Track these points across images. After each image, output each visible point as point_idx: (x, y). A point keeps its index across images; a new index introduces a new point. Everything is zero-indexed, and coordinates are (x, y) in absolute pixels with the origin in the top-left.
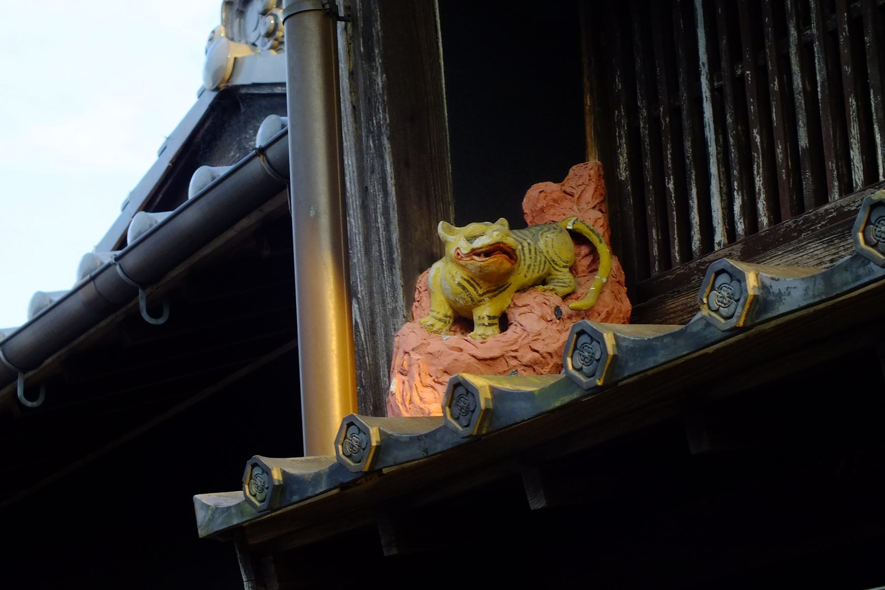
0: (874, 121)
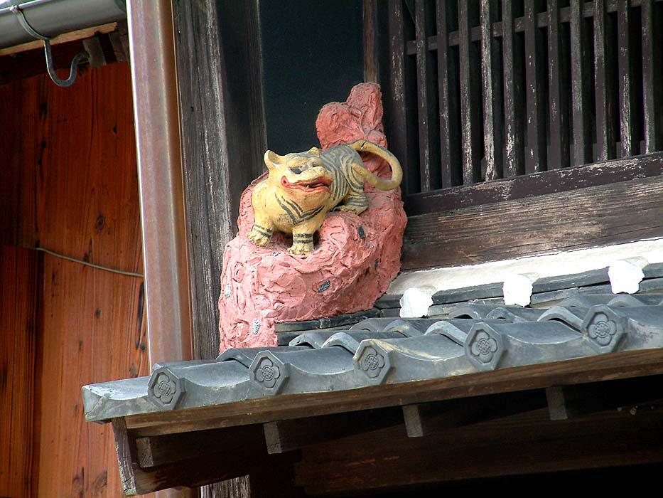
0: (645, 101)
